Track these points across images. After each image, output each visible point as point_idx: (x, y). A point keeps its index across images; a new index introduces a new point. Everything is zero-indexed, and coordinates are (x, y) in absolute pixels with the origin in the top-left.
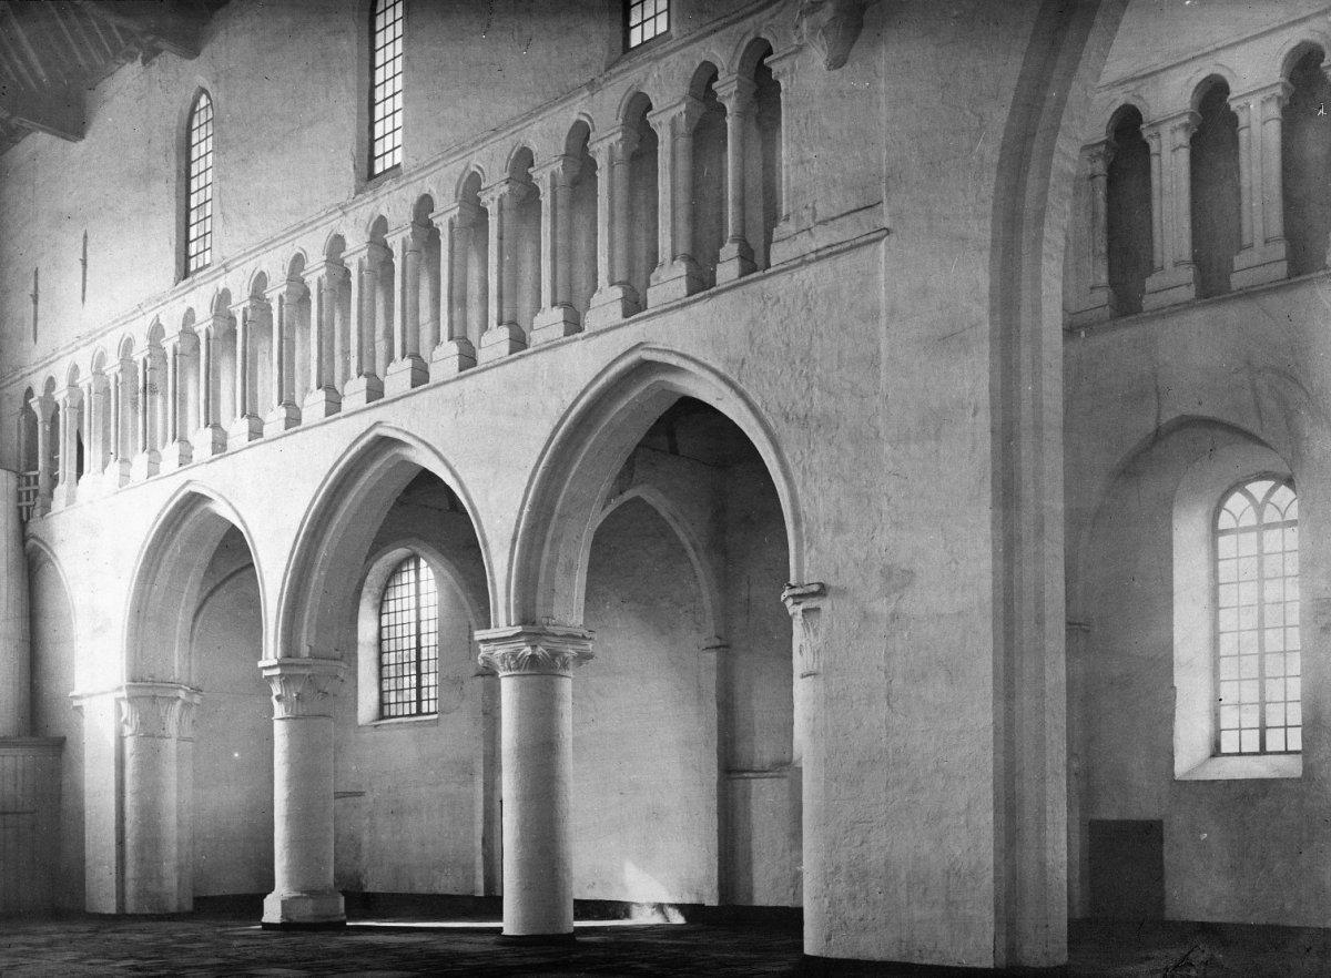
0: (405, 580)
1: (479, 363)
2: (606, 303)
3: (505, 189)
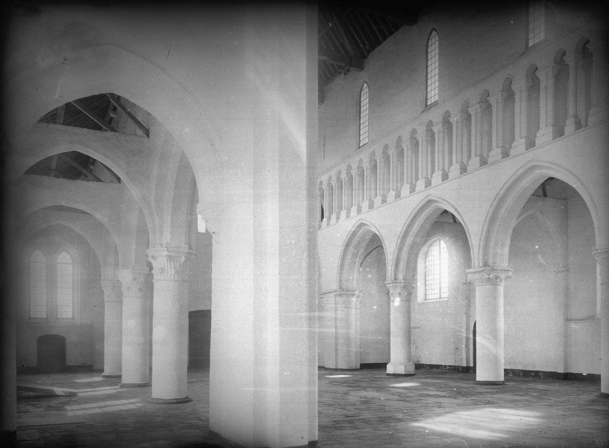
0: (435, 249)
1: (536, 145)
2: (421, 184)
3: (478, 105)
